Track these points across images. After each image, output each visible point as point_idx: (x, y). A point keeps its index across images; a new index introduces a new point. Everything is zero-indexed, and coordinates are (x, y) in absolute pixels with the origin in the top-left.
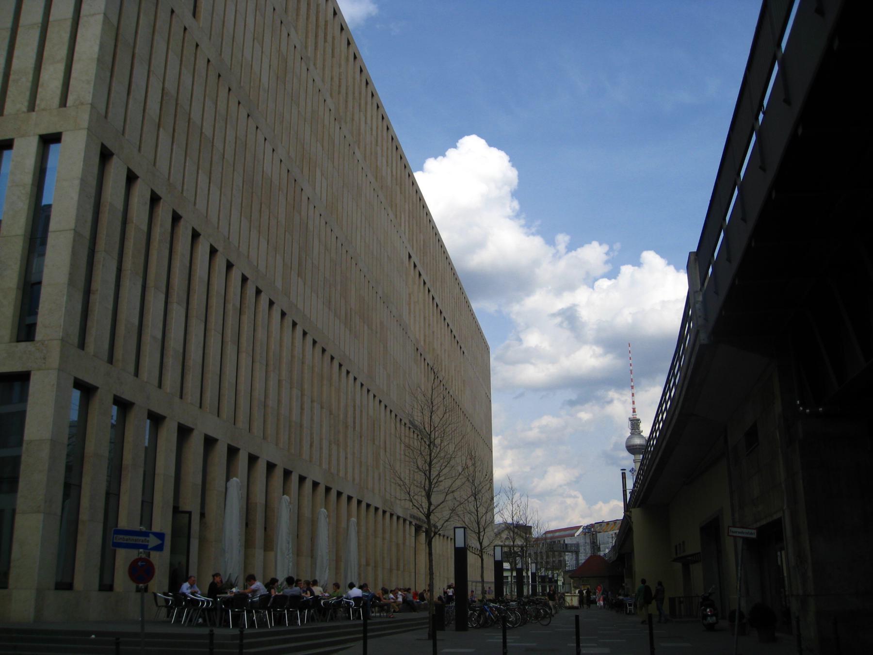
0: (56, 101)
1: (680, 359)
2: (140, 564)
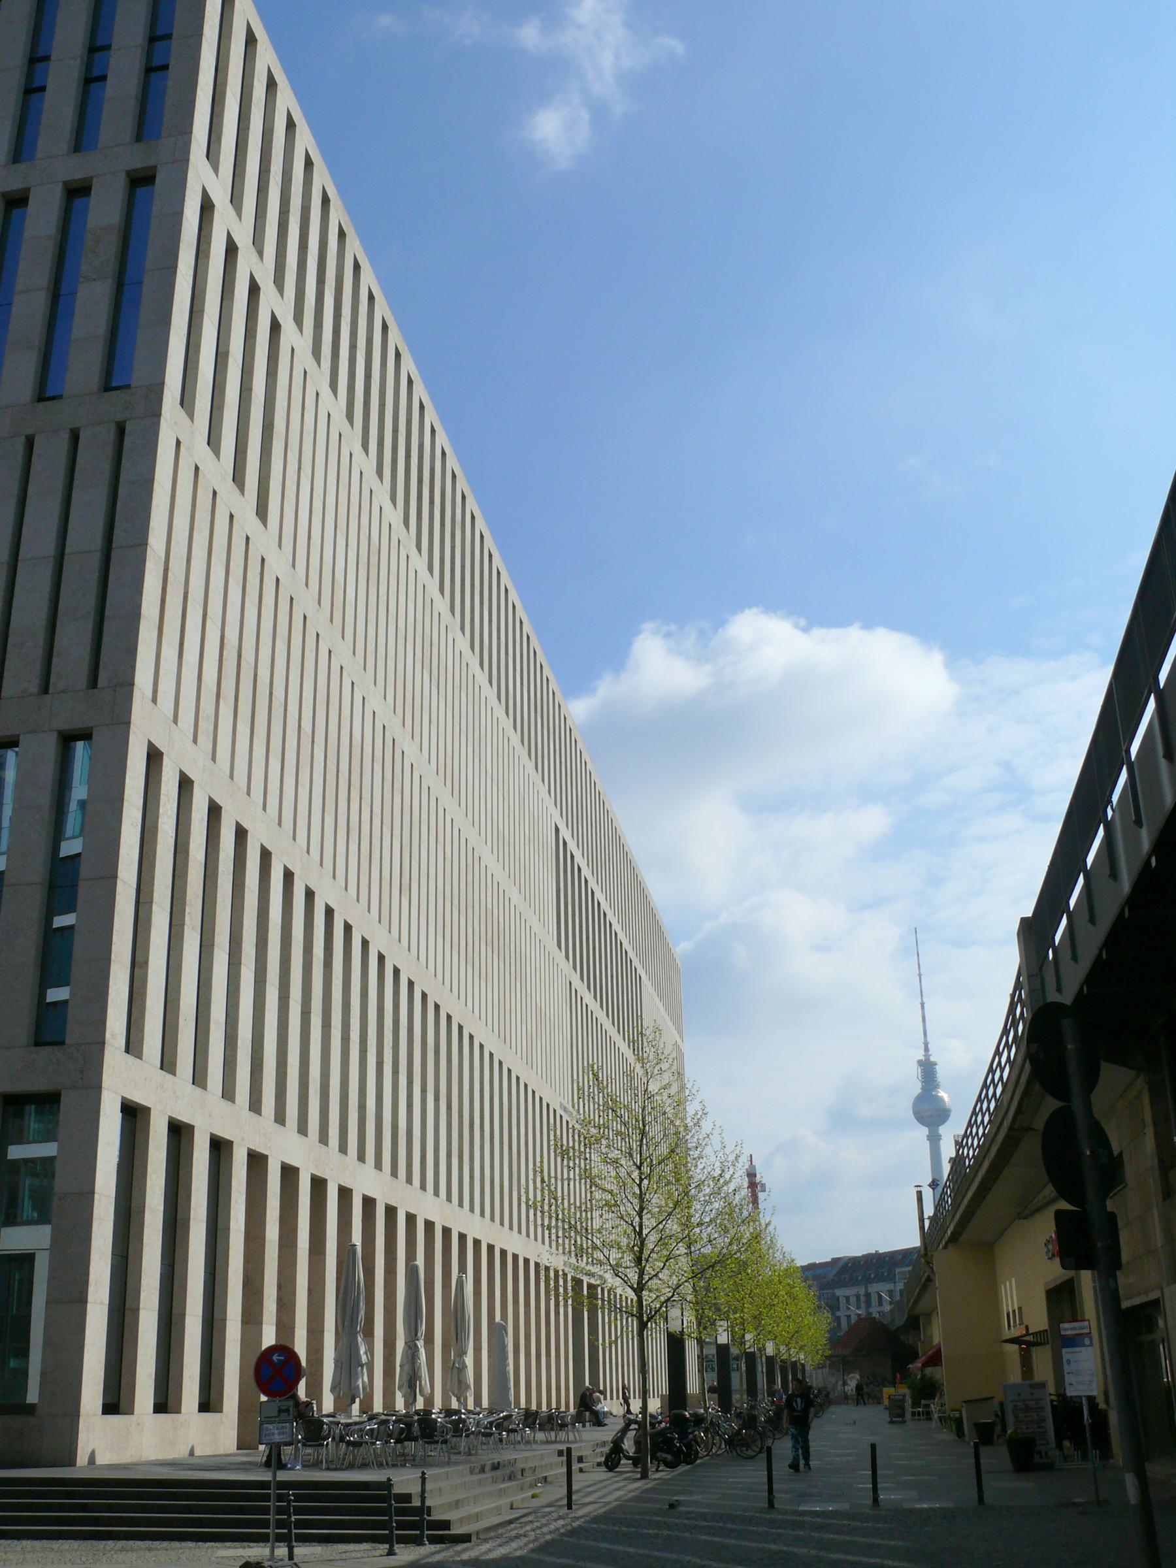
0: (82, 679)
1: (1015, 1024)
2: (275, 1358)
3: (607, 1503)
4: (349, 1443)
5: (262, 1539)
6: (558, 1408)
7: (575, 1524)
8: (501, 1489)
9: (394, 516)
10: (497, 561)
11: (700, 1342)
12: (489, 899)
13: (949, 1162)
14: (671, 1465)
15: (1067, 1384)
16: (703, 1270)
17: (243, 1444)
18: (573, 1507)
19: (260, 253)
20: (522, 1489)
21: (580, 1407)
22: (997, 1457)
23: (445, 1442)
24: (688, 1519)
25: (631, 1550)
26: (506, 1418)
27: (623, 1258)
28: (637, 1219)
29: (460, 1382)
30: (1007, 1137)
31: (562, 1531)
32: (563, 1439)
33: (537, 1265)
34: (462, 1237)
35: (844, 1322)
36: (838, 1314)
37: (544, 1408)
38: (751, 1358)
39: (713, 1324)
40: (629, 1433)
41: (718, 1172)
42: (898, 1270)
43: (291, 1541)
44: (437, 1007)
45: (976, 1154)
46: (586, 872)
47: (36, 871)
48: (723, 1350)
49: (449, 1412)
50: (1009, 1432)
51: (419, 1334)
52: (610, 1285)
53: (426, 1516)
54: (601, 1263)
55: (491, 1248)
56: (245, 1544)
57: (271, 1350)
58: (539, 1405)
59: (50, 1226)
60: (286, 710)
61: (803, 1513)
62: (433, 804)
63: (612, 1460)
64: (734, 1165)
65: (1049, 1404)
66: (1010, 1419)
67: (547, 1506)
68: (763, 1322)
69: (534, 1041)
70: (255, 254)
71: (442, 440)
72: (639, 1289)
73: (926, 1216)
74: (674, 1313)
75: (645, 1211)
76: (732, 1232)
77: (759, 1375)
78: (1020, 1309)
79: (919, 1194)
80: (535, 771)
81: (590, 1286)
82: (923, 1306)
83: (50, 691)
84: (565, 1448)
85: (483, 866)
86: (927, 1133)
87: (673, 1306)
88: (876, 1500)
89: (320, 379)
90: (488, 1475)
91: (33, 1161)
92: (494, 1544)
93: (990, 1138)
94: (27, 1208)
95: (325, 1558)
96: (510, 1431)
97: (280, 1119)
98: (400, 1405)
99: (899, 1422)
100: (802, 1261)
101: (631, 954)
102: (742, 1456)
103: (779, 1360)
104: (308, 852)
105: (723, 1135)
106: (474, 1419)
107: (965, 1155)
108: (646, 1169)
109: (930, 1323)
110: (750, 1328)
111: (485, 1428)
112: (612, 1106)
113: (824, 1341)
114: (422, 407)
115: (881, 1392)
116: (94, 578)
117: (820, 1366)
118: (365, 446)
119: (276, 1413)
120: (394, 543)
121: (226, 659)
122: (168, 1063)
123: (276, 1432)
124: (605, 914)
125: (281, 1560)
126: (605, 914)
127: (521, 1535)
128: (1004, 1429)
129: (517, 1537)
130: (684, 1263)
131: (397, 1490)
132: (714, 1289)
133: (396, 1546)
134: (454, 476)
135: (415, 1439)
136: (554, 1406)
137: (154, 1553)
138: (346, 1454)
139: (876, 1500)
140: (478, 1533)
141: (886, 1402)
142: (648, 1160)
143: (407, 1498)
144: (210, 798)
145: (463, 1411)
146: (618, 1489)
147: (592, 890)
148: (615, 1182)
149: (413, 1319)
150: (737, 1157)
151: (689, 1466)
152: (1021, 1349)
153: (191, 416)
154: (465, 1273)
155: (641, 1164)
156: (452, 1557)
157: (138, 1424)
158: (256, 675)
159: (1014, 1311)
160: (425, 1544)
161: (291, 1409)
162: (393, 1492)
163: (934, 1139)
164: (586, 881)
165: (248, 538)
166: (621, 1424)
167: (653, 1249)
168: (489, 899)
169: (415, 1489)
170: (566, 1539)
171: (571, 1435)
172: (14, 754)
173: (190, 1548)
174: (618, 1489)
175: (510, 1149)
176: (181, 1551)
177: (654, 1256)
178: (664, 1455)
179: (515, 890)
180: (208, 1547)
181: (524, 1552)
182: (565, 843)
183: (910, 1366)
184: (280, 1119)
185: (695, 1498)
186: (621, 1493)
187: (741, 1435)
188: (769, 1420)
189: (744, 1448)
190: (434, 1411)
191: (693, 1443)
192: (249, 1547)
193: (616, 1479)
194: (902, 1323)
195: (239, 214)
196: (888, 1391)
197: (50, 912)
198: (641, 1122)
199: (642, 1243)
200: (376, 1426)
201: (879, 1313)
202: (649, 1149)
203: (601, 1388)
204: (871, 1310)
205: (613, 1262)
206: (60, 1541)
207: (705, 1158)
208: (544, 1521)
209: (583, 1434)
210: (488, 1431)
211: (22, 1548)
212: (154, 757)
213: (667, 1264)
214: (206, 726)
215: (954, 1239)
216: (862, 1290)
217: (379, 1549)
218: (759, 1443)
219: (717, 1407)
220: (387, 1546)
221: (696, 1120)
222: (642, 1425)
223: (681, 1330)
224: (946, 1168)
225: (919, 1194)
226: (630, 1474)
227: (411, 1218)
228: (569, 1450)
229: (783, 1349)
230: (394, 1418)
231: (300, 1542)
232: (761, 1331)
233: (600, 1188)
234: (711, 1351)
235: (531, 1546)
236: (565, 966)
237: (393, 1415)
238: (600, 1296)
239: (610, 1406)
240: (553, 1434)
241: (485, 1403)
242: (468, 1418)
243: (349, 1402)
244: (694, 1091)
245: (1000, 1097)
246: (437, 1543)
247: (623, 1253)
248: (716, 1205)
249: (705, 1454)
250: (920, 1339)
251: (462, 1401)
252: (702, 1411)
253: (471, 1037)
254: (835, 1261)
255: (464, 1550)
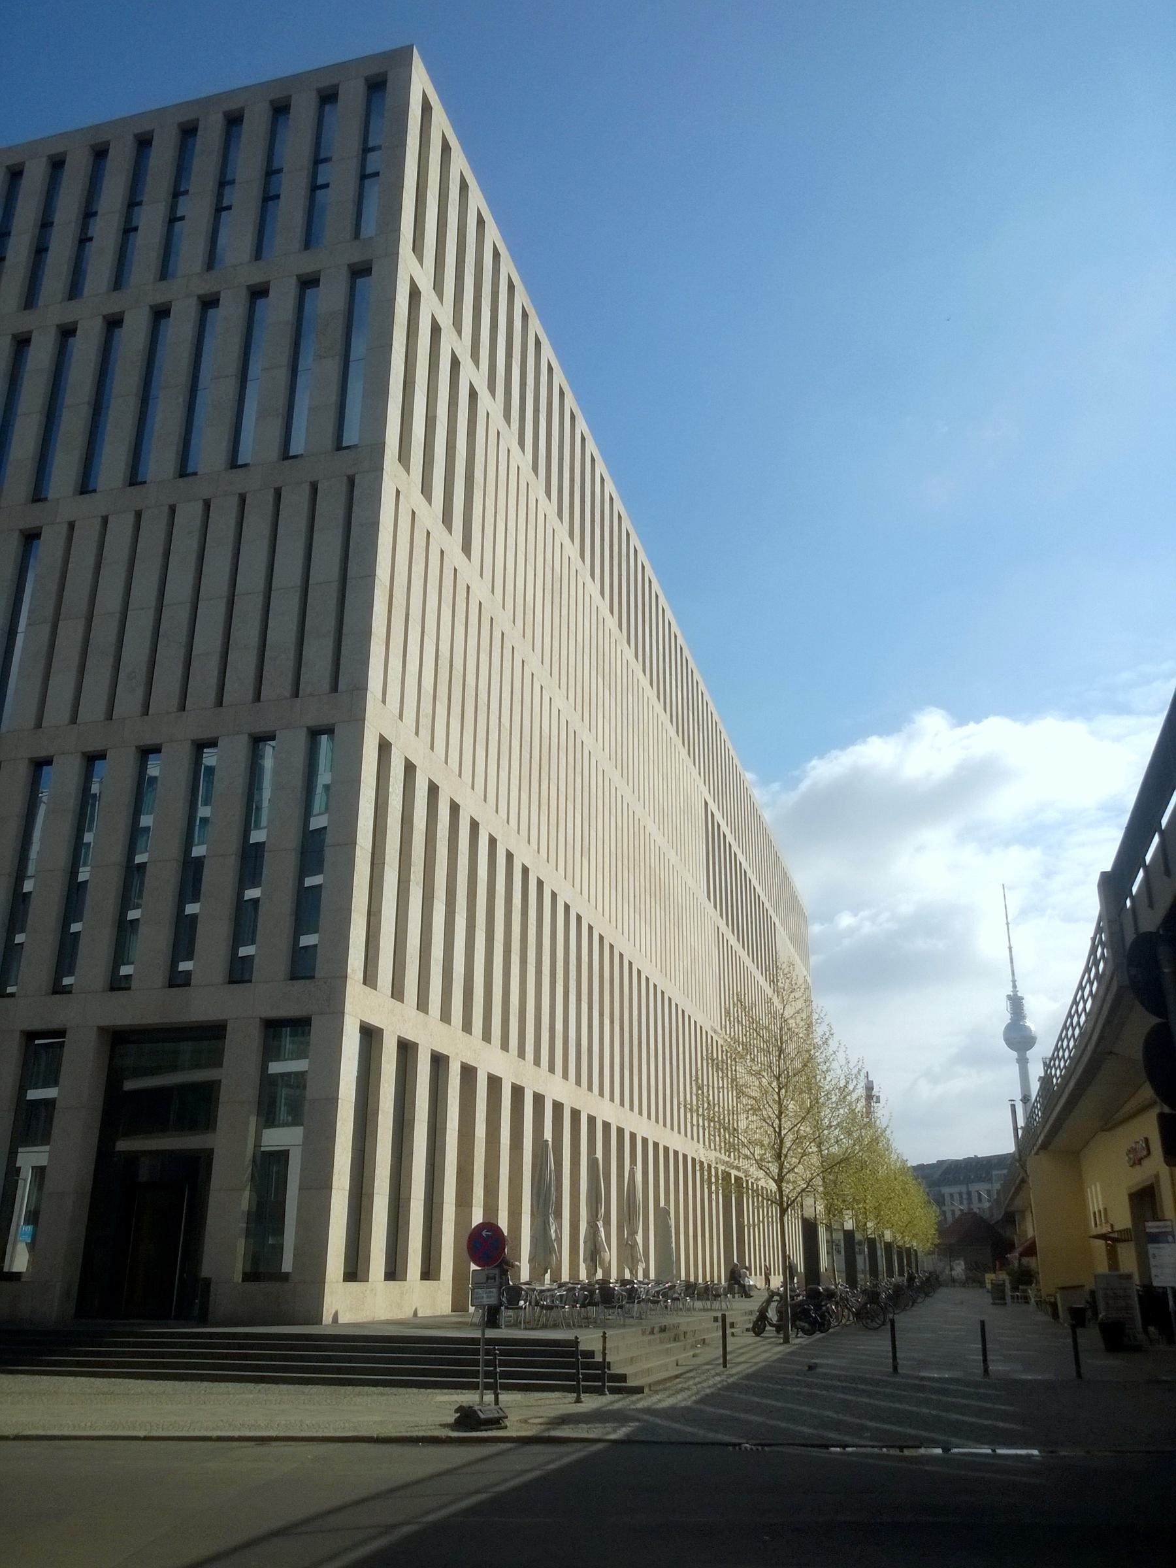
0: (326, 685)
1: (1096, 964)
3: (756, 1363)
4: (543, 1307)
5: (474, 1387)
6: (712, 1281)
7: (731, 1380)
8: (668, 1348)
9: (572, 550)
10: (656, 586)
11: (829, 1228)
12: (652, 861)
13: (1039, 1081)
14: (809, 1333)
15: (1153, 1275)
16: (832, 1167)
17: (458, 1305)
18: (728, 1365)
19: (459, 332)
20: (684, 1350)
21: (730, 1280)
22: (1091, 1336)
23: (621, 1307)
24: (824, 1379)
25: (779, 1404)
26: (670, 1288)
27: (765, 1154)
28: (777, 1121)
29: (633, 1257)
30: (1091, 1060)
31: (719, 1386)
32: (717, 1308)
33: (693, 1160)
34: (633, 1136)
35: (949, 1216)
36: (944, 1208)
37: (700, 1281)
38: (872, 1243)
39: (841, 1212)
40: (772, 1304)
41: (842, 1084)
42: (994, 1173)
43: (497, 1389)
44: (612, 947)
45: (1062, 1073)
46: (730, 838)
47: (292, 838)
48: (849, 1235)
49: (624, 1283)
50: (1100, 1316)
51: (599, 1216)
52: (755, 1177)
53: (606, 1370)
54: (747, 1157)
55: (656, 1145)
56: (459, 1391)
57: (480, 1227)
58: (696, 1277)
59: (302, 1128)
60: (489, 708)
61: (923, 1379)
62: (607, 783)
63: (759, 1326)
64: (857, 1078)
65: (1136, 1293)
66: (1101, 1306)
67: (707, 1364)
68: (882, 1213)
69: (690, 976)
70: (455, 334)
71: (610, 487)
72: (780, 1180)
73: (1019, 1127)
74: (809, 1201)
75: (783, 1115)
76: (855, 1135)
77: (879, 1259)
78: (1105, 1209)
79: (1013, 1107)
80: (688, 756)
81: (737, 1178)
82: (1018, 1203)
83: (300, 695)
84: (720, 1315)
85: (647, 833)
86: (1016, 1057)
87: (808, 1195)
88: (986, 1370)
89: (510, 437)
90: (658, 1336)
91: (289, 1074)
92: (663, 1396)
93: (1075, 1061)
94: (283, 1113)
95: (524, 1404)
96: (674, 1299)
97: (487, 1037)
98: (583, 1275)
99: (1001, 1304)
100: (912, 1163)
101: (767, 905)
102: (866, 1327)
103: (895, 1246)
104: (508, 822)
105: (847, 1053)
106: (644, 1288)
107: (1053, 1074)
108: (783, 1080)
109: (1024, 1218)
110: (872, 1216)
111: (654, 1296)
112: (756, 1027)
113: (933, 1231)
114: (593, 460)
115: (983, 1276)
116: (333, 603)
117: (930, 1253)
118: (548, 493)
119: (484, 1281)
120: (573, 573)
121: (440, 668)
122: (397, 993)
123: (485, 1296)
124: (745, 872)
125: (489, 1405)
126: (745, 872)
127: (686, 1389)
128: (1096, 1313)
129: (682, 1390)
130: (815, 1160)
131: (582, 1347)
132: (841, 1183)
133: (582, 1395)
134: (620, 517)
135: (596, 1304)
136: (708, 1279)
137: (384, 1398)
138: (540, 1317)
139: (986, 1370)
140: (650, 1385)
141: (989, 1286)
142: (786, 1072)
143: (591, 1354)
144: (429, 779)
145: (635, 1281)
146: (765, 1351)
147: (712, 812)
148: (758, 1090)
149: (594, 1205)
150: (859, 1071)
151: (823, 1334)
152: (1108, 1245)
153: (407, 470)
154: (636, 1165)
155: (780, 1075)
156: (629, 1405)
157: (372, 1290)
158: (464, 681)
159: (1100, 1211)
160: (606, 1394)
161: (497, 1276)
162: (580, 1349)
163: (1023, 1062)
164: (730, 845)
165: (455, 570)
166: (766, 1295)
167: (790, 1147)
168: (652, 861)
169: (597, 1347)
170: (721, 1392)
171: (723, 1303)
172: (272, 749)
173: (414, 1394)
174: (765, 1351)
175: (671, 1063)
176: (407, 1396)
177: (791, 1153)
178: (803, 1324)
179: (673, 853)
180: (429, 1394)
181: (689, 1403)
182: (712, 815)
183: (1009, 1255)
184: (487, 1037)
185: (830, 1362)
186: (768, 1355)
187: (866, 1308)
188: (889, 1297)
189: (870, 1321)
190: (611, 1281)
191: (826, 1314)
192: (462, 1393)
193: (764, 1343)
194: (1000, 1217)
195: (441, 299)
196: (989, 1277)
197: (303, 873)
198: (779, 1040)
199: (782, 1142)
200: (565, 1293)
201: (979, 1208)
202: (786, 1063)
203: (747, 1265)
204: (972, 1206)
205: (758, 1157)
206: (309, 1386)
207: (832, 1071)
208: (704, 1377)
209: (734, 1304)
210: (655, 1299)
211: (280, 1391)
212: (385, 747)
213: (802, 1160)
214: (425, 722)
215: (1045, 1146)
216: (964, 1189)
217: (568, 1397)
218: (881, 1317)
219: (845, 1284)
220: (575, 1395)
221: (824, 1040)
222: (783, 1297)
223: (814, 1216)
224: (1035, 1087)
225: (1013, 1107)
226: (773, 1340)
227: (592, 1120)
228: (724, 1316)
229: (899, 1237)
230: (579, 1286)
231: (504, 1390)
232: (880, 1220)
233: (746, 1095)
234: (839, 1236)
235: (694, 1398)
236: (714, 914)
237: (579, 1284)
238: (745, 1186)
239: (754, 1280)
240: (709, 1303)
241: (652, 1276)
242: (640, 1288)
243: (542, 1272)
244: (822, 1015)
245: (1084, 1024)
246: (616, 1393)
247: (766, 1150)
248: (841, 1111)
249: (836, 1324)
250: (1016, 1234)
251: (633, 1272)
252: (833, 1287)
253: (639, 972)
254: (940, 1163)
255: (639, 1400)
